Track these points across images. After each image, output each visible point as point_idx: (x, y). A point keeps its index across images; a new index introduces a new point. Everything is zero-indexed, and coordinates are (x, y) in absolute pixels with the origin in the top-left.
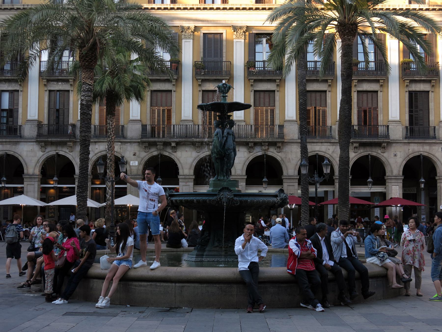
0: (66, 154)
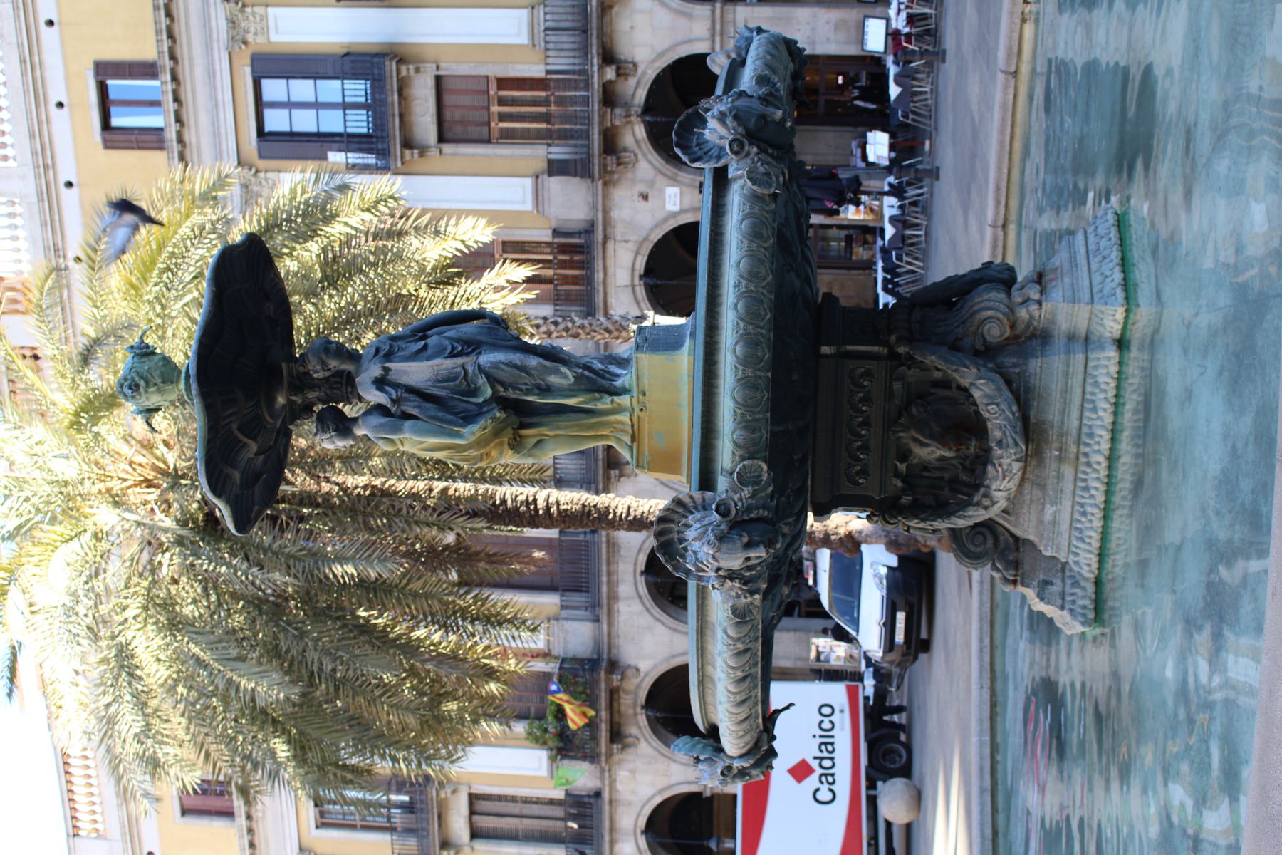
0: (644, 80)
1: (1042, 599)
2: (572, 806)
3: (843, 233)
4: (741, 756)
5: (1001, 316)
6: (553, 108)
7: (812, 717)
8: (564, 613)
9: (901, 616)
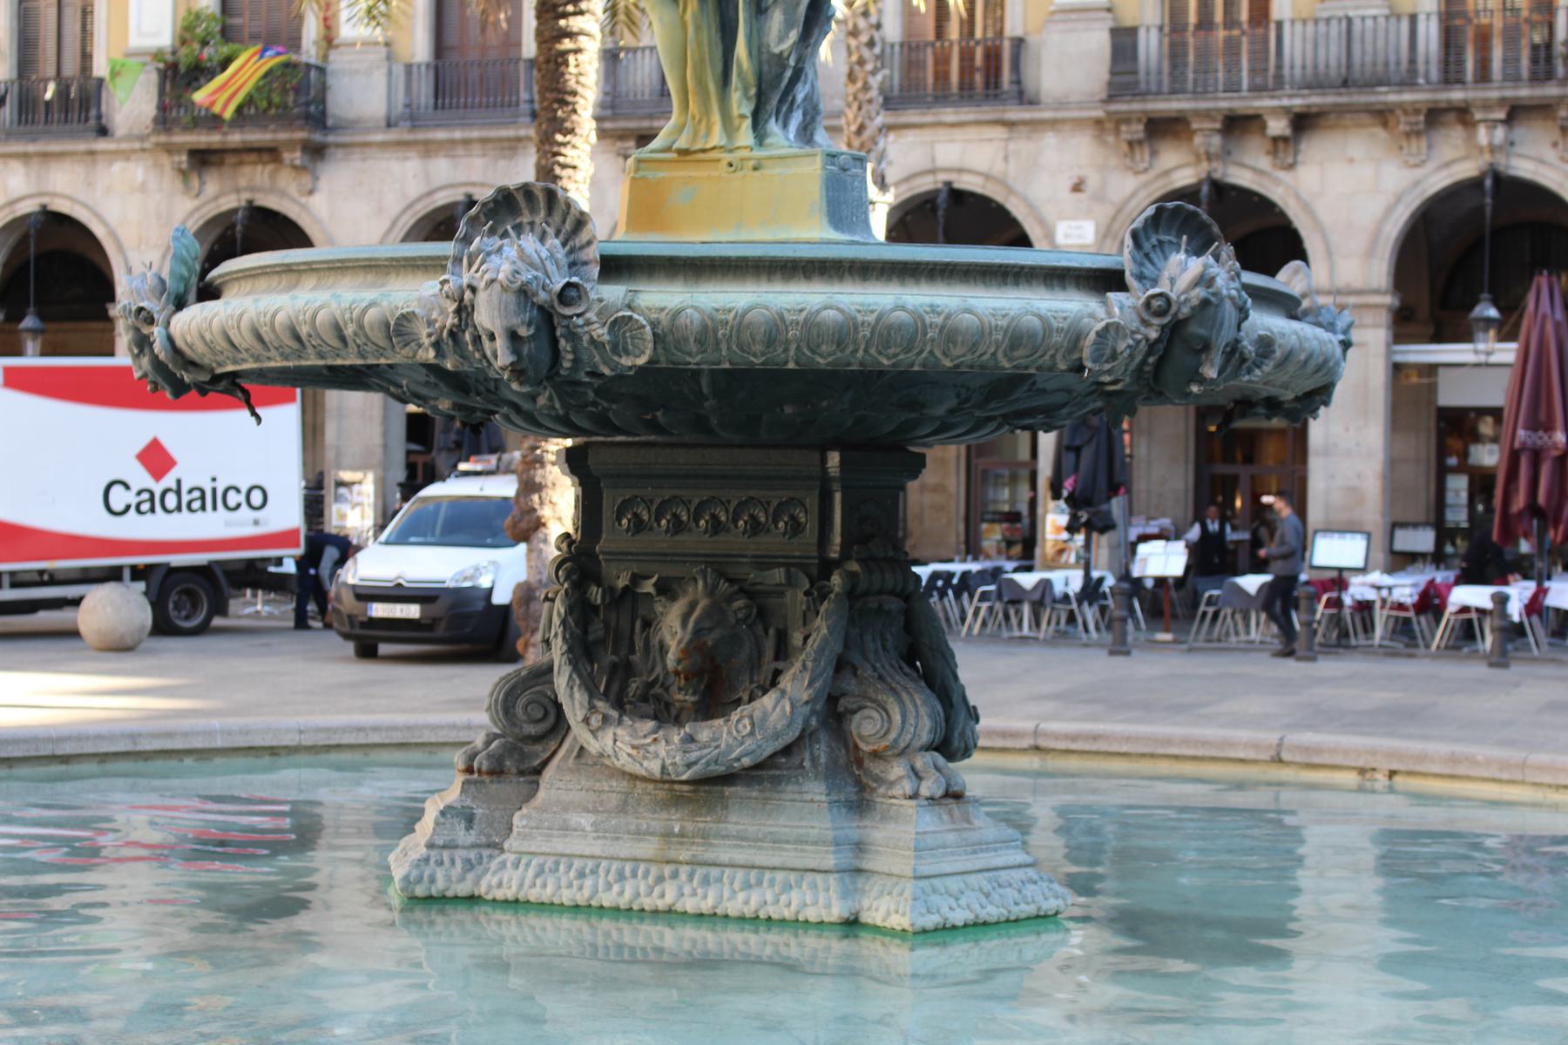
0: (1267, 182)
1: (443, 813)
2: (81, 89)
3: (1023, 508)
4: (170, 339)
5: (893, 735)
6: (1221, 34)
7: (244, 470)
8: (399, 70)
9: (412, 611)
